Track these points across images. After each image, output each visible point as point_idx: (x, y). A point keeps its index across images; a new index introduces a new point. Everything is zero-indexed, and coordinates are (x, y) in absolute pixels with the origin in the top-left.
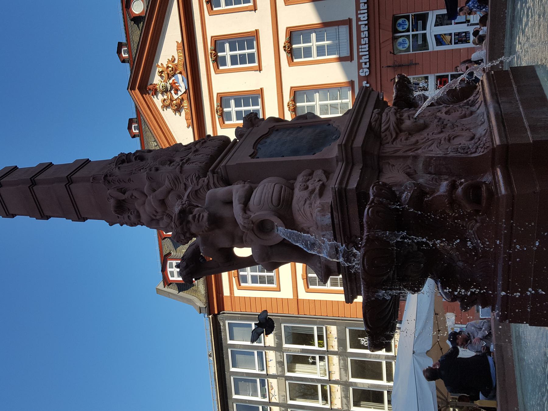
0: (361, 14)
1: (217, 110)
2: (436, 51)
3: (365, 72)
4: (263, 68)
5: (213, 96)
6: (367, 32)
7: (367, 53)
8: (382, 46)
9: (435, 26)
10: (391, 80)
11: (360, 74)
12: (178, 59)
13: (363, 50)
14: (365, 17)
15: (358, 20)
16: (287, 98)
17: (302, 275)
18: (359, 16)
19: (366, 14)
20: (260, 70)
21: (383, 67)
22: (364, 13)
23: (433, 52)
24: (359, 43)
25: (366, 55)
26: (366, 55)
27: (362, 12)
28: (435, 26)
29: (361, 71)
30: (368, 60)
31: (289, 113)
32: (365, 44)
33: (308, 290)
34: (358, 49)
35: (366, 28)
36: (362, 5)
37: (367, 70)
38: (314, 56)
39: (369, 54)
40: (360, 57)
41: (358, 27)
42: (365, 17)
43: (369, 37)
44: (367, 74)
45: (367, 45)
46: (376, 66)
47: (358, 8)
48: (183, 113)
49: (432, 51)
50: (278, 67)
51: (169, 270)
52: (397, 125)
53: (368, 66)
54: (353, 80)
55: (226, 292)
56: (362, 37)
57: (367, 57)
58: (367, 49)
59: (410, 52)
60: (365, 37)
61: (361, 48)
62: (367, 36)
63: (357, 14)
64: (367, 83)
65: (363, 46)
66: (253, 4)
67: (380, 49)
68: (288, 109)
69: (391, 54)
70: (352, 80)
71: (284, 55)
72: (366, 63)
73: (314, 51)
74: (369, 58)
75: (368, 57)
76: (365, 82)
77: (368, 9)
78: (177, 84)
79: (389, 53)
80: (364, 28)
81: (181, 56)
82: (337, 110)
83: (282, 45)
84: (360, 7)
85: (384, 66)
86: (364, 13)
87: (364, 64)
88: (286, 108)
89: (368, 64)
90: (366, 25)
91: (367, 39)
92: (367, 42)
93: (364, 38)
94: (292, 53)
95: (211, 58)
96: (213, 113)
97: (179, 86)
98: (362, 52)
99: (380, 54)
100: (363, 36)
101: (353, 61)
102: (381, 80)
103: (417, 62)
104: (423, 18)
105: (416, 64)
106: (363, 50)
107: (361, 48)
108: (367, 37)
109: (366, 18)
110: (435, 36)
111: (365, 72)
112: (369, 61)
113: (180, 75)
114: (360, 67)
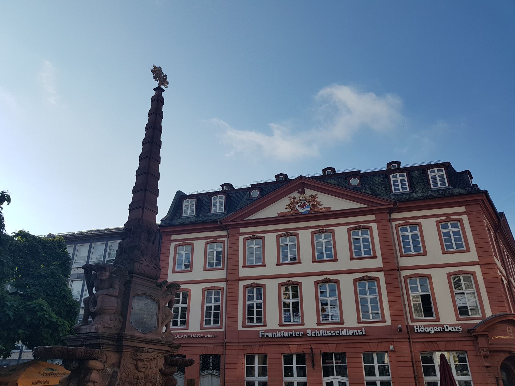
0: (346, 330)
1: (288, 233)
2: (322, 382)
3: (309, 334)
4: (352, 261)
5: (332, 227)
6: (335, 335)
7: (321, 335)
8: (287, 346)
9: (339, 381)
10: (303, 351)
11: (308, 330)
12: (320, 208)
13: (323, 332)
14: (344, 333)
15: (343, 329)
16: (294, 280)
17: (214, 286)
18: (345, 330)
19: (346, 334)
20: (313, 262)
21: (311, 346)
22: (346, 333)
23: (322, 380)
24: (328, 329)
25: (320, 334)
26: (320, 334)
27: (348, 331)
28: (339, 381)
29: (310, 331)
30: (317, 335)
31: (285, 281)
32: (327, 334)
33: (245, 287)
34: (324, 329)
35: (337, 334)
36: (298, 333)
37: (310, 335)
38: (256, 301)
39: (320, 336)
40: (319, 330)
41: (338, 329)
42: (344, 333)
43: (331, 336)
44: (308, 335)
45: (326, 335)
46: (340, 340)
47: (350, 329)
48: (288, 210)
49: (364, 379)
50: (185, 283)
51: (436, 169)
52: (139, 359)
53: (313, 335)
54: (344, 324)
55: (174, 237)
56: (359, 331)
57: (319, 335)
58: (324, 335)
59: (323, 364)
60: (331, 334)
61: (324, 331)
62: (332, 335)
63: (346, 328)
64: (302, 335)
65: (325, 332)
66: (354, 257)
67: (324, 344)
68: (364, 275)
69: (320, 352)
70: (386, 321)
71: (322, 278)
72: (315, 334)
73: (295, 300)
74: (318, 336)
75: (318, 335)
76: (303, 334)
77: (349, 335)
78: (304, 207)
79: (321, 349)
80: (337, 333)
81: (322, 210)
82: (208, 317)
83: (255, 281)
84: (297, 332)
85: (311, 346)
86: (346, 333)
87: (314, 332)
88: (288, 279)
89: (315, 335)
90: (339, 334)
91: (330, 335)
92: (328, 335)
93: (331, 332)
94: (286, 285)
95: (358, 226)
96: (286, 230)
97: (303, 208)
98: (322, 331)
99: (343, 343)
100: (332, 332)
101: (317, 325)
102: (233, 345)
103: (315, 369)
104: (344, 375)
105: (314, 368)
106: (323, 332)
107: (324, 331)
108: (331, 335)
109: (343, 334)
110: (332, 382)
111: (309, 334)
112: (316, 336)
113: (310, 209)
114: (313, 330)
